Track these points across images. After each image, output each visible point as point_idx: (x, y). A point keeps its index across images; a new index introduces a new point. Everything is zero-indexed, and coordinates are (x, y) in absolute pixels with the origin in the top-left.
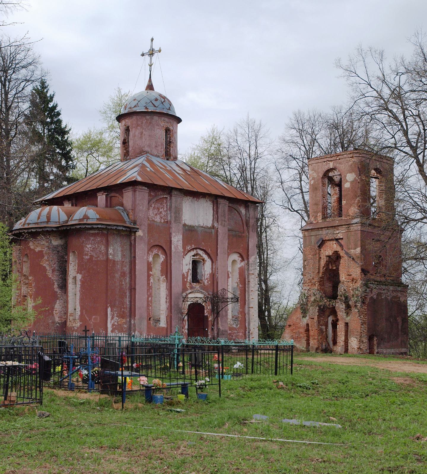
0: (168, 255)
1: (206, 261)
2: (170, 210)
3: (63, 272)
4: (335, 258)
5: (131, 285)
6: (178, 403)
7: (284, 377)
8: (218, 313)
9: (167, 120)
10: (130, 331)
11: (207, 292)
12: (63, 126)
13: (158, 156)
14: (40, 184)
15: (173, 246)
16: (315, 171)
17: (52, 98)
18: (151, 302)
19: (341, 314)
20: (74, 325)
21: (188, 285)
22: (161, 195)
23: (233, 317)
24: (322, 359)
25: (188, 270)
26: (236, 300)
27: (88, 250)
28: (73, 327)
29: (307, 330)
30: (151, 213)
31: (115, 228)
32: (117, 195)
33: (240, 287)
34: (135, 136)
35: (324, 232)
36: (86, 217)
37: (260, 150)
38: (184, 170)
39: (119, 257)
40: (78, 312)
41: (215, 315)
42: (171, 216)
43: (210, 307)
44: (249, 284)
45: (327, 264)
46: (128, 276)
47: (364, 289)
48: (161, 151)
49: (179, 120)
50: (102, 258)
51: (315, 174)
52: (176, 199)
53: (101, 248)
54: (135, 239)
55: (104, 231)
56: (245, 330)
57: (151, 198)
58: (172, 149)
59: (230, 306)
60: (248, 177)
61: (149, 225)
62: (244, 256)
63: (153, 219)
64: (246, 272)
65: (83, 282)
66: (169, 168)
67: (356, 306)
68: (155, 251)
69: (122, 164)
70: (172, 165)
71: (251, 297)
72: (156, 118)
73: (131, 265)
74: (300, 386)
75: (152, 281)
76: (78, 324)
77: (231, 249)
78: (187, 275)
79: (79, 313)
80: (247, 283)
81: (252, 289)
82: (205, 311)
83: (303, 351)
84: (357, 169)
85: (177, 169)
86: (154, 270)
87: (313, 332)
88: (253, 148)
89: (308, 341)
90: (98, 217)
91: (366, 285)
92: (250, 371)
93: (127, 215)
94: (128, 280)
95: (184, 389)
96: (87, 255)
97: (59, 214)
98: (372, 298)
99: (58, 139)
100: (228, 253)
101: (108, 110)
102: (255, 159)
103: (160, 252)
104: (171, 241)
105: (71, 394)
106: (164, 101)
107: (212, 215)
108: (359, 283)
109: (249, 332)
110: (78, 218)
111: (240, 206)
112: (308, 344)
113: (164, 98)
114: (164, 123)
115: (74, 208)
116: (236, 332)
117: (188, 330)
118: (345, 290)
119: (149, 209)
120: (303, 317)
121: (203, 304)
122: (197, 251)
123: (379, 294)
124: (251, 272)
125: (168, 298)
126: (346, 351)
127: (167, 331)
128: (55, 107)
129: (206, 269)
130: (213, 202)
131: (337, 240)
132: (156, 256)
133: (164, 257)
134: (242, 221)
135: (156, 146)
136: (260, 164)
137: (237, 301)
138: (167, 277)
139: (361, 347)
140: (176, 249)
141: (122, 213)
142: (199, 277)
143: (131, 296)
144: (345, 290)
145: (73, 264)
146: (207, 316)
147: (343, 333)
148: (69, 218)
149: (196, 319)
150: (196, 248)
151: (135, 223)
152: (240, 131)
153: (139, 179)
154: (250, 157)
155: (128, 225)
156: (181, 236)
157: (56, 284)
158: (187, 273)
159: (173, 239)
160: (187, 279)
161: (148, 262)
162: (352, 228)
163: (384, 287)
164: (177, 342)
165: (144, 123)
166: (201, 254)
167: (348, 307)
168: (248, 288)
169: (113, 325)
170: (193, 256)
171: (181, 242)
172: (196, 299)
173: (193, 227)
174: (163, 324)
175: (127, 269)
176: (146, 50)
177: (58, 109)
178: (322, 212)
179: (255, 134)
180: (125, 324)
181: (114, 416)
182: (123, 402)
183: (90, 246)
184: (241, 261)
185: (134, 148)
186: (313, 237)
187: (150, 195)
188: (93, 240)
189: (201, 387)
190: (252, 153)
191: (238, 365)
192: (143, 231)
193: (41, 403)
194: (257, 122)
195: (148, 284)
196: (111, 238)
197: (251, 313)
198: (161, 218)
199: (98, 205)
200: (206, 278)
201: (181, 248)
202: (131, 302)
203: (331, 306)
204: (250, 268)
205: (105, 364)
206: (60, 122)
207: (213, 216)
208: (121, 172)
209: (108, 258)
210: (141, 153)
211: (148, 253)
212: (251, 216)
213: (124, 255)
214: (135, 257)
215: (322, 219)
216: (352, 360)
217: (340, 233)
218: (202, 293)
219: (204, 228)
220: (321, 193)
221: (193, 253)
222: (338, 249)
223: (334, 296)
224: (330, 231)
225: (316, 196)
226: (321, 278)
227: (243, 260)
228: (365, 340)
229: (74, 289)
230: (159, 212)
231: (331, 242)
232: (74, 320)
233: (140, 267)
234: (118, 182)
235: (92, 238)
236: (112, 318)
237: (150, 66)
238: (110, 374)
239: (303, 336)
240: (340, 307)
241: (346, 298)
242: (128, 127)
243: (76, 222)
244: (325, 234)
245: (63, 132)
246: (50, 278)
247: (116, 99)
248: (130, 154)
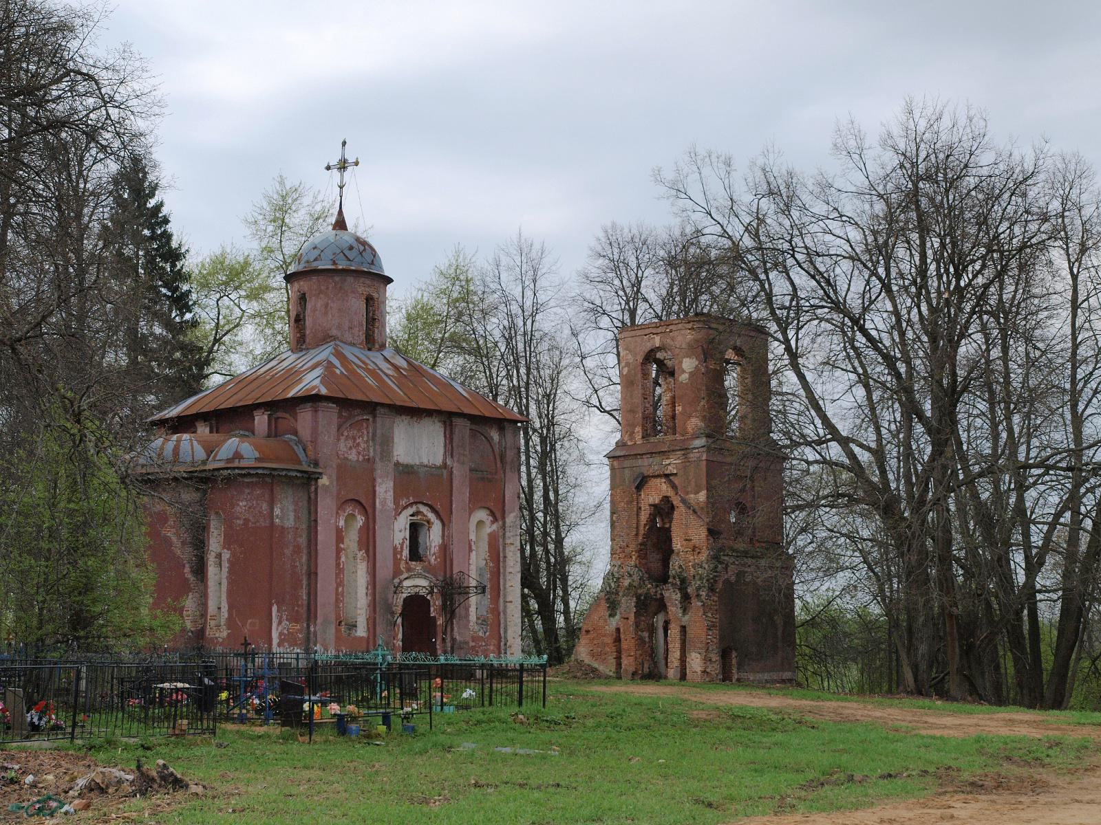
0: (371, 516)
2: (373, 440)
3: (199, 545)
4: (664, 509)
5: (309, 566)
6: (378, 736)
7: (529, 707)
8: (453, 613)
9: (368, 282)
10: (308, 642)
11: (435, 576)
12: (174, 244)
13: (354, 345)
14: (129, 357)
15: (377, 501)
16: (630, 351)
17: (154, 188)
18: (343, 596)
19: (674, 609)
21: (403, 566)
22: (358, 415)
23: (478, 618)
24: (649, 691)
26: (482, 589)
29: (618, 640)
30: (342, 446)
31: (284, 473)
32: (287, 416)
34: (314, 310)
35: (646, 461)
36: (237, 455)
37: (542, 297)
38: (396, 368)
39: (290, 522)
40: (225, 613)
42: (374, 450)
43: (439, 602)
45: (652, 520)
46: (305, 551)
47: (712, 566)
49: (389, 280)
50: (263, 523)
51: (630, 356)
52: (383, 421)
54: (316, 489)
55: (268, 479)
56: (500, 641)
58: (376, 330)
59: (473, 600)
60: (522, 350)
61: (339, 467)
62: (498, 514)
64: (501, 540)
65: (233, 564)
66: (372, 366)
67: (698, 596)
68: (349, 510)
69: (294, 357)
70: (376, 358)
71: (508, 584)
72: (350, 279)
73: (309, 533)
74: (547, 721)
75: (343, 559)
76: (225, 634)
77: (476, 502)
78: (402, 548)
79: (226, 615)
81: (511, 570)
82: (432, 609)
83: (608, 677)
84: (700, 349)
85: (385, 366)
86: (346, 540)
87: (628, 643)
88: (529, 293)
89: (618, 659)
90: (257, 455)
91: (716, 558)
92: (486, 703)
93: (304, 450)
94: (304, 559)
95: (386, 720)
96: (239, 519)
97: (192, 449)
98: (727, 582)
99: (163, 268)
101: (261, 217)
102: (533, 316)
104: (375, 491)
105: (243, 728)
106: (365, 250)
108: (704, 556)
109: (505, 644)
110: (225, 457)
111: (491, 427)
112: (619, 665)
113: (364, 243)
114: (362, 287)
115: (215, 436)
117: (402, 641)
118: (680, 567)
119: (339, 440)
120: (610, 615)
121: (428, 597)
123: (740, 575)
124: (508, 541)
126: (683, 677)
127: (368, 643)
128: (159, 207)
129: (434, 537)
130: (445, 423)
131: (667, 476)
132: (351, 517)
134: (493, 451)
136: (545, 323)
137: (484, 592)
138: (367, 552)
139: (708, 670)
140: (383, 506)
141: (295, 447)
142: (421, 551)
143: (309, 585)
144: (680, 567)
145: (216, 532)
146: (435, 617)
147: (678, 645)
148: (209, 456)
149: (418, 621)
150: (416, 503)
151: (316, 464)
152: (505, 261)
153: (324, 391)
154: (523, 311)
155: (305, 468)
156: (392, 484)
157: (187, 565)
159: (377, 488)
161: (337, 527)
162: (692, 455)
163: (750, 561)
164: (380, 659)
166: (425, 513)
167: (686, 598)
168: (505, 567)
169: (281, 634)
170: (412, 515)
172: (417, 590)
173: (412, 466)
174: (361, 632)
175: (303, 541)
176: (334, 161)
177: (165, 211)
178: (643, 426)
179: (532, 275)
180: (301, 633)
181: (300, 748)
182: (311, 735)
183: (244, 503)
184: (493, 522)
186: (627, 471)
187: (340, 416)
189: (407, 717)
190: (528, 303)
191: (468, 693)
192: (330, 477)
193: (214, 733)
194: (537, 246)
195: (338, 565)
196: (277, 489)
197: (508, 611)
198: (359, 453)
199: (256, 432)
200: (432, 552)
201: (390, 504)
202: (309, 594)
203: (658, 596)
204: (508, 534)
205: (285, 687)
206: (167, 236)
207: (445, 446)
208: (292, 375)
209: (272, 523)
210: (325, 339)
211: (337, 513)
212: (508, 445)
213: (299, 518)
214: (316, 521)
215: (643, 437)
216: (668, 690)
217: (672, 464)
218: (425, 578)
219: (430, 467)
220: (641, 391)
221: (410, 511)
222: (670, 493)
223: (663, 579)
224: (657, 459)
225: (631, 396)
226: (641, 544)
227: (495, 520)
228: (715, 657)
229: (217, 576)
231: (658, 480)
232: (218, 626)
233: (325, 536)
234: (290, 395)
235: (247, 491)
236: (280, 623)
237: (341, 187)
238: (295, 700)
239: (611, 650)
240: (672, 596)
241: (683, 581)
242: (304, 294)
243: (221, 465)
244: (648, 465)
245: (174, 256)
247: (275, 196)
248: (307, 341)
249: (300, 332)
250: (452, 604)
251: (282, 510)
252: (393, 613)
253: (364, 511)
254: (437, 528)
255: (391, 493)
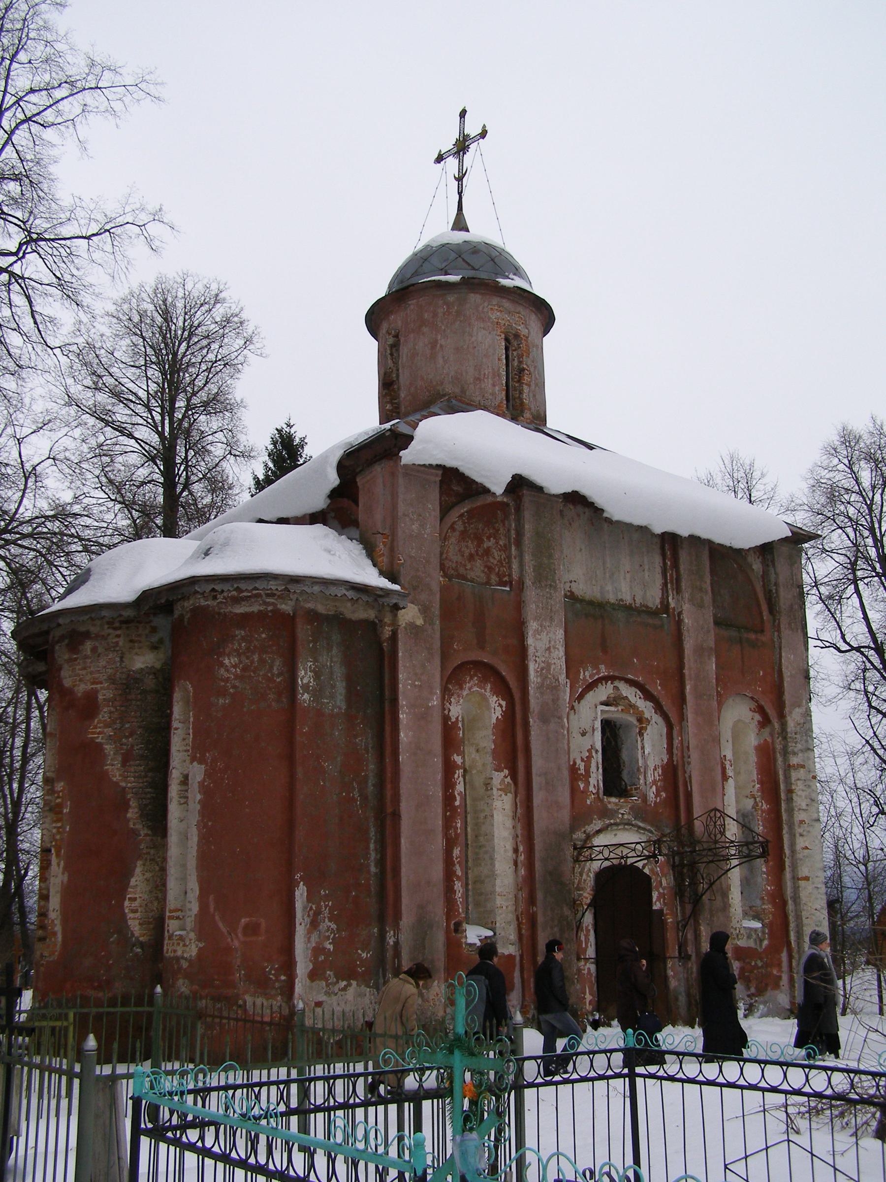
0: (517, 696)
1: (648, 721)
8: (697, 901)
9: (507, 304)
15: (532, 667)
20: (179, 953)
25: (589, 751)
27: (226, 675)
28: (178, 959)
33: (763, 811)
41: (689, 908)
44: (790, 800)
48: (493, 394)
53: (271, 667)
57: (453, 499)
58: (526, 389)
63: (462, 571)
71: (800, 843)
76: (193, 951)
80: (783, 796)
82: (655, 895)
86: (470, 753)
100: (719, 694)
103: (489, 687)
107: (658, 570)
114: (498, 313)
116: (760, 964)
117: (598, 962)
122: (616, 688)
125: (521, 849)
129: (649, 750)
133: (504, 703)
135: (479, 379)
138: (514, 775)
146: (661, 911)
150: (612, 678)
156: (560, 634)
157: (133, 803)
158: (588, 761)
159: (530, 641)
160: (588, 783)
165: (440, 315)
166: (633, 699)
168: (790, 811)
169: (318, 950)
171: (561, 652)
176: (448, 144)
183: (234, 660)
185: (412, 389)
188: (243, 639)
195: (448, 799)
197: (803, 895)
198: (490, 569)
202: (381, 862)
204: (791, 746)
212: (781, 579)
221: (604, 692)
230: (481, 552)
236: (314, 924)
237: (459, 179)
242: (396, 336)
246: (117, 783)
249: (391, 403)
250: (694, 883)
251: (317, 675)
252: (574, 904)
253: (502, 688)
254: (655, 731)
255: (560, 653)
